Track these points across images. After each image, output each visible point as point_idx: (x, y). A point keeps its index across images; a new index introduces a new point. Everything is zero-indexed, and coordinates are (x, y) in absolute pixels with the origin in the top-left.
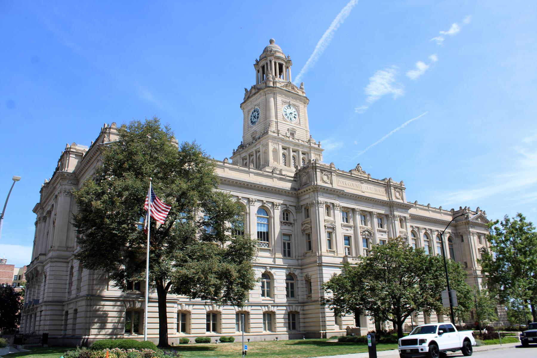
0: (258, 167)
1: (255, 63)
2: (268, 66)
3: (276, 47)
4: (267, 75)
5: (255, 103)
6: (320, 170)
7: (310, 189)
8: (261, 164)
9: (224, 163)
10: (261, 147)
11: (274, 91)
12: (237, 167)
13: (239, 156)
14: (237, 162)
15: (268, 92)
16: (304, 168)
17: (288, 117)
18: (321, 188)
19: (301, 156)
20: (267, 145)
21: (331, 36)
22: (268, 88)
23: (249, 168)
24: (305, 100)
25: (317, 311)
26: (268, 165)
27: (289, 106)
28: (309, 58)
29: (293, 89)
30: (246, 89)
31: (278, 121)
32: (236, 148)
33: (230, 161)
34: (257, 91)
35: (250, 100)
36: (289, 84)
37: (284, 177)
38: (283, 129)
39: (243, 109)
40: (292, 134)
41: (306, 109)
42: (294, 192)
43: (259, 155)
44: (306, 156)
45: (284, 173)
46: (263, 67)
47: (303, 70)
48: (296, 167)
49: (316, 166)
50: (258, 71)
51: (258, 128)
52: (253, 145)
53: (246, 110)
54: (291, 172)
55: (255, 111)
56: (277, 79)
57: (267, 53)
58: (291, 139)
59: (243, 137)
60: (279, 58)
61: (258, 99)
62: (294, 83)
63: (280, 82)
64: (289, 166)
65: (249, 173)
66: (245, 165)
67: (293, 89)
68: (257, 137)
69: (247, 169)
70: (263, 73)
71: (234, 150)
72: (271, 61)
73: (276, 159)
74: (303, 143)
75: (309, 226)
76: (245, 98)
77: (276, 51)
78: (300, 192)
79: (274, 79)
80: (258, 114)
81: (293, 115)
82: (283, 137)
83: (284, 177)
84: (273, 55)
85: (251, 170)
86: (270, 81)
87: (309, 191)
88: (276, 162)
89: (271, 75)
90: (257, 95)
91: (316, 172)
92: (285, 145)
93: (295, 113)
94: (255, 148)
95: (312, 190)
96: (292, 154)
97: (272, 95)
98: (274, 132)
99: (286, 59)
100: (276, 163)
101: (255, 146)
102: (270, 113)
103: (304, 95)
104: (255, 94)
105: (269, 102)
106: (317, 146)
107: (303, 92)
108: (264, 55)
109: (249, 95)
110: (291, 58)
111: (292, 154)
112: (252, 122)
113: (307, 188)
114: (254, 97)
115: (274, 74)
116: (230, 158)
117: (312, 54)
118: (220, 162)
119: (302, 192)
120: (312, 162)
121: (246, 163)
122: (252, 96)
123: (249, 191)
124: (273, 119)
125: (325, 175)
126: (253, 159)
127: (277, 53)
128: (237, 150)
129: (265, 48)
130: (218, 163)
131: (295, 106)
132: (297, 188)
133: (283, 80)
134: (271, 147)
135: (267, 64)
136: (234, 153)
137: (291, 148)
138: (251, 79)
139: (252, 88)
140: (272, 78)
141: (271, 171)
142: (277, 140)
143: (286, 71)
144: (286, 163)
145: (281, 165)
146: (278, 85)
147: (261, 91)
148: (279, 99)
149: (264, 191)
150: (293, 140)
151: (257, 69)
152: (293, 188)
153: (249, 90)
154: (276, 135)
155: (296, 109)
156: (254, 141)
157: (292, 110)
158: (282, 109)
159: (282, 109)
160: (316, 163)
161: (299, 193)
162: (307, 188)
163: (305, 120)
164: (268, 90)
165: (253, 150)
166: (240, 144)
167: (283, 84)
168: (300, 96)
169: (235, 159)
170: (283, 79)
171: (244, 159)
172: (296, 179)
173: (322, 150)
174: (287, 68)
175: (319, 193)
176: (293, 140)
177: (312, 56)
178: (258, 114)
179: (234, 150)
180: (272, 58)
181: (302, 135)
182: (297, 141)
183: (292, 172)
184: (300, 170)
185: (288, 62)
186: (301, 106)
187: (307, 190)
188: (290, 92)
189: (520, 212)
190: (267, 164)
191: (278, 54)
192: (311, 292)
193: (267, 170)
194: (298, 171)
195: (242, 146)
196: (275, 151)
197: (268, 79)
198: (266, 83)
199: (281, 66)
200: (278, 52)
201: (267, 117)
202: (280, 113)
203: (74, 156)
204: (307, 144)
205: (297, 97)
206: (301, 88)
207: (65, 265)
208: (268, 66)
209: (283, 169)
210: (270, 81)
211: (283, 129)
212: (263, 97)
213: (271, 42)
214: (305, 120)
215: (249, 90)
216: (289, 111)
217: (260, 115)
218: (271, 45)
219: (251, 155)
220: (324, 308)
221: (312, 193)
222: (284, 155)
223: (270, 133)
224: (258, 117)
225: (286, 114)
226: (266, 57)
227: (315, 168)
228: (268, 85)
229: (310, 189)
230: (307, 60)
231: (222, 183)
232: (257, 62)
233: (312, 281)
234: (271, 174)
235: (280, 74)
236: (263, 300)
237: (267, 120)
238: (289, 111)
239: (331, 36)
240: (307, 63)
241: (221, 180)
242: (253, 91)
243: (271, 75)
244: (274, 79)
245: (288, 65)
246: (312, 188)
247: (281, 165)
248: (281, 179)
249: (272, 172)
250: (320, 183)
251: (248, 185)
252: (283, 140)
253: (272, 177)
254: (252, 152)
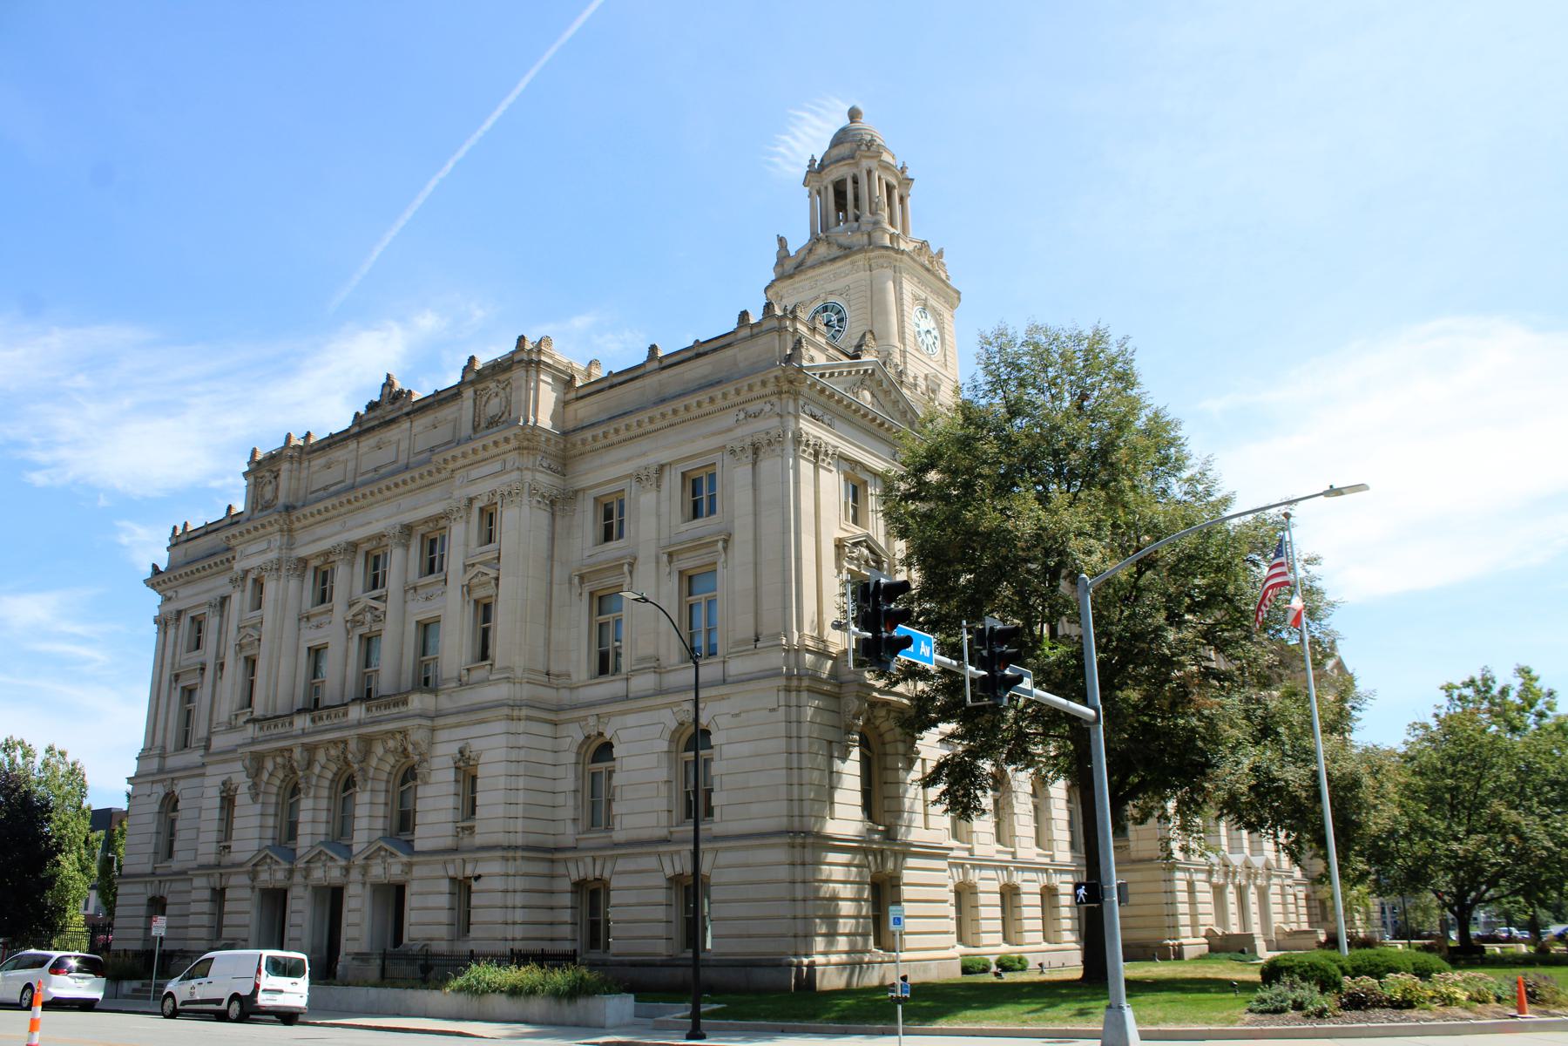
5: (830, 287)
6: (554, 378)
7: (507, 440)
25: (1152, 887)
72: (869, 172)
75: (493, 574)
90: (839, 264)
91: (538, 382)
105: (883, 291)
122: (813, 267)
124: (895, 341)
148: (908, 287)
162: (499, 437)
178: (840, 320)
180: (873, 164)
189: (1524, 664)
192: (474, 813)
202: (910, 331)
207: (546, 729)
220: (1171, 880)
229: (507, 440)
233: (481, 772)
236: (998, 852)
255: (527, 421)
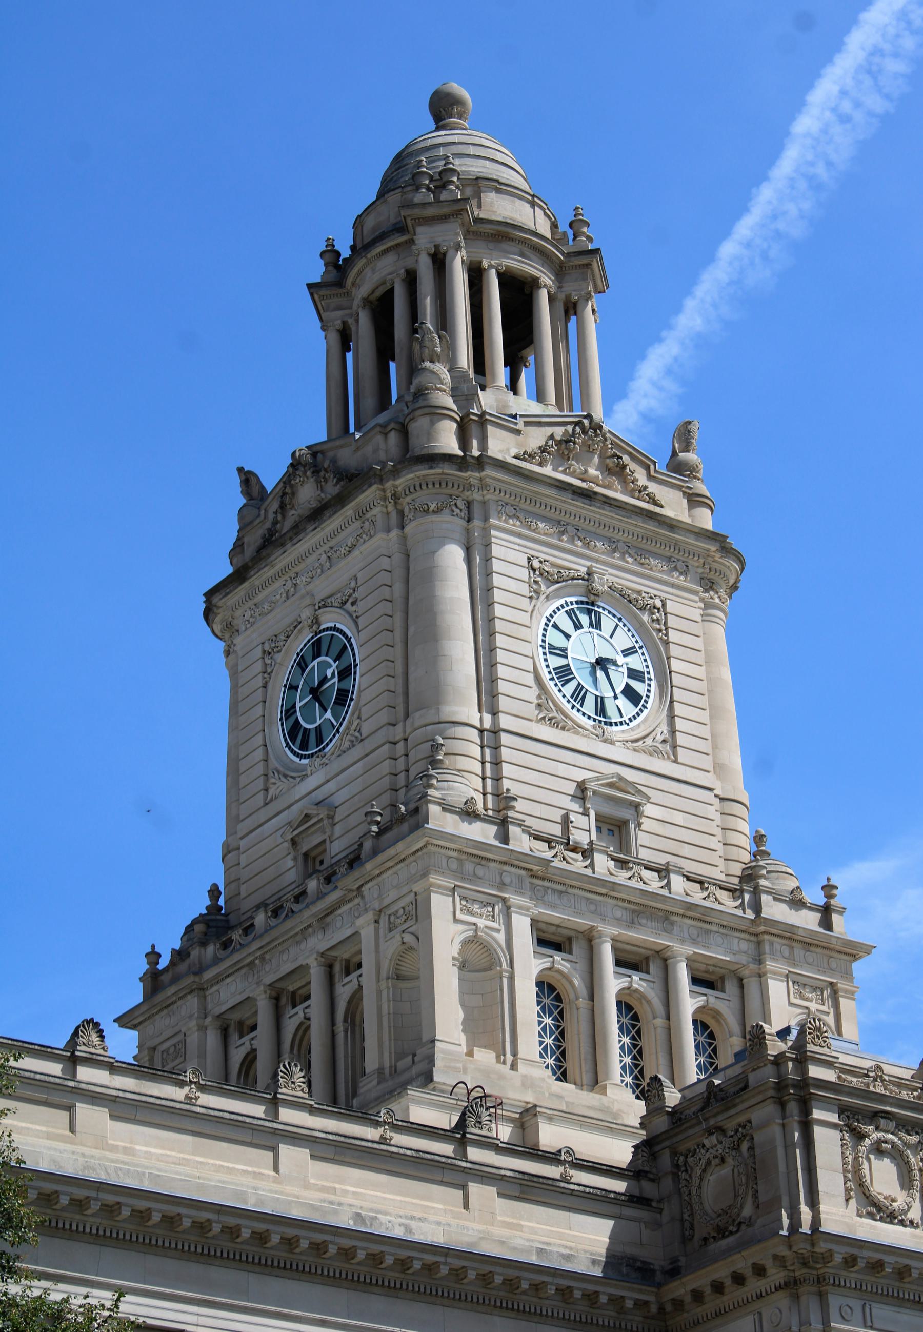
0: (345, 1092)
1: (317, 271)
2: (416, 298)
3: (480, 150)
4: (412, 370)
5: (322, 587)
6: (843, 1110)
7: (760, 1271)
8: (371, 1063)
9: (72, 1060)
10: (367, 933)
11: (468, 489)
12: (178, 1093)
13: (192, 1002)
14: (180, 1051)
15: (421, 497)
16: (711, 1100)
17: (579, 695)
18: (850, 1262)
19: (689, 1003)
20: (418, 913)
21: (909, 43)
22: (422, 472)
23: (274, 1103)
24: (712, 562)
26: (427, 1078)
27: (589, 605)
28: (743, 209)
29: (618, 471)
30: (248, 479)
31: (505, 722)
32: (169, 942)
33: (124, 1044)
34: (332, 489)
35: (282, 559)
36: (582, 435)
37: (553, 1171)
38: (543, 786)
39: (228, 633)
40: (617, 828)
41: (719, 632)
42: (631, 1294)
43: (356, 999)
44: (723, 1003)
45: (550, 1136)
46: (381, 308)
47: (690, 304)
48: (648, 1090)
49: (805, 1083)
50: (345, 339)
51: (342, 780)
52: (308, 915)
53: (250, 639)
54: (603, 1128)
55: (316, 648)
56: (487, 400)
57: (416, 195)
58: (603, 864)
59: (228, 850)
60: (503, 234)
61: (341, 557)
62: (621, 421)
63: (518, 419)
64: (595, 1082)
65: (268, 1138)
66: (244, 1078)
67: (618, 471)
68: (337, 848)
69: (258, 1110)
70: (385, 350)
71: (153, 956)
72: (440, 262)
73: (488, 1023)
74: (697, 896)
76: (238, 546)
77: (479, 184)
78: (680, 1289)
79: (464, 395)
80: (345, 673)
81: (620, 680)
82: (541, 850)
83: (553, 1171)
84: (457, 210)
85: (287, 1115)
86: (437, 413)
87: (755, 1285)
88: (482, 1052)
89: (442, 370)
90: (332, 523)
91: (807, 1127)
92: (558, 915)
93: (635, 661)
94: (320, 942)
95: (776, 1276)
96: (613, 983)
97: (451, 522)
98: (469, 814)
99: (558, 238)
100: (485, 1057)
101: (324, 920)
102: (435, 659)
103: (705, 520)
104: (317, 514)
106: (808, 920)
107: (694, 500)
108: (388, 213)
109: (271, 523)
110: (597, 235)
111: (613, 983)
112: (294, 731)
113: (741, 1262)
114: (311, 539)
115: (465, 359)
116: (124, 1021)
117: (761, 177)
118: (44, 1052)
119: (698, 1296)
120: (775, 1047)
121: (250, 1059)
122: (298, 530)
123: (276, 1284)
124: (466, 708)
125: (878, 1150)
126: (304, 1029)
127: (490, 197)
128: (179, 955)
129: (400, 160)
130: (28, 1063)
131: (630, 605)
132: (656, 1257)
133: (535, 408)
134: (447, 930)
135: (411, 279)
136: (154, 981)
137: (609, 934)
138: (283, 398)
139: (296, 464)
140: (455, 393)
141: (446, 1120)
142: (490, 872)
143: (560, 337)
144: (567, 1058)
145: (525, 1075)
146: (501, 445)
147: (370, 494)
148: (510, 553)
149: (392, 1289)
150: (622, 877)
151: (336, 318)
152: (617, 1261)
153: (270, 480)
154: (482, 833)
155: (640, 629)
156: (312, 885)
157: (614, 639)
158: (530, 626)
159: (530, 626)
160: (802, 1058)
161: (678, 1304)
162: (741, 1262)
163: (715, 711)
164: (423, 484)
165: (308, 953)
166: (200, 905)
167: (536, 438)
168: (671, 525)
169: (163, 1024)
170: (540, 397)
171: (233, 1026)
172: (649, 1189)
173: (853, 951)
174: (569, 309)
175: (835, 1301)
176: (622, 877)
177: (766, 194)
178: (345, 673)
179: (153, 956)
180: (449, 234)
181: (692, 831)
182: (654, 883)
183: (612, 1128)
184: (676, 1114)
185: (579, 264)
186: (683, 607)
187: (739, 1279)
188: (596, 499)
190: (415, 1063)
191: (499, 208)
193: (421, 1114)
194: (661, 1124)
195: (216, 927)
196: (483, 965)
197: (418, 397)
198: (404, 432)
199: (519, 294)
200: (499, 187)
201: (414, 694)
203: (834, 1118)
204: (728, 904)
205: (651, 538)
206: (678, 467)
208: (416, 298)
209: (545, 1102)
210: (437, 413)
211: (543, 786)
212: (384, 542)
213: (443, 108)
214: (715, 711)
215: (270, 480)
216: (583, 647)
217: (360, 679)
218: (443, 136)
219: (286, 997)
221: (782, 1300)
222: (547, 988)
223: (439, 820)
224: (343, 697)
225: (564, 674)
226: (400, 228)
227: (796, 1094)
228: (418, 445)
230: (726, 234)
231: (54, 1228)
232: (338, 268)
234: (447, 1149)
235: (514, 362)
237: (418, 718)
238: (583, 647)
239: (909, 43)
240: (728, 249)
241: (47, 1199)
242: (307, 493)
243: (442, 370)
244: (464, 395)
245: (572, 289)
246: (779, 1260)
247: (525, 1075)
248: (525, 1189)
249: (459, 1135)
250: (839, 1216)
251: (261, 1238)
252: (538, 878)
253: (454, 1175)
254: (302, 969)
255: (795, 1225)
